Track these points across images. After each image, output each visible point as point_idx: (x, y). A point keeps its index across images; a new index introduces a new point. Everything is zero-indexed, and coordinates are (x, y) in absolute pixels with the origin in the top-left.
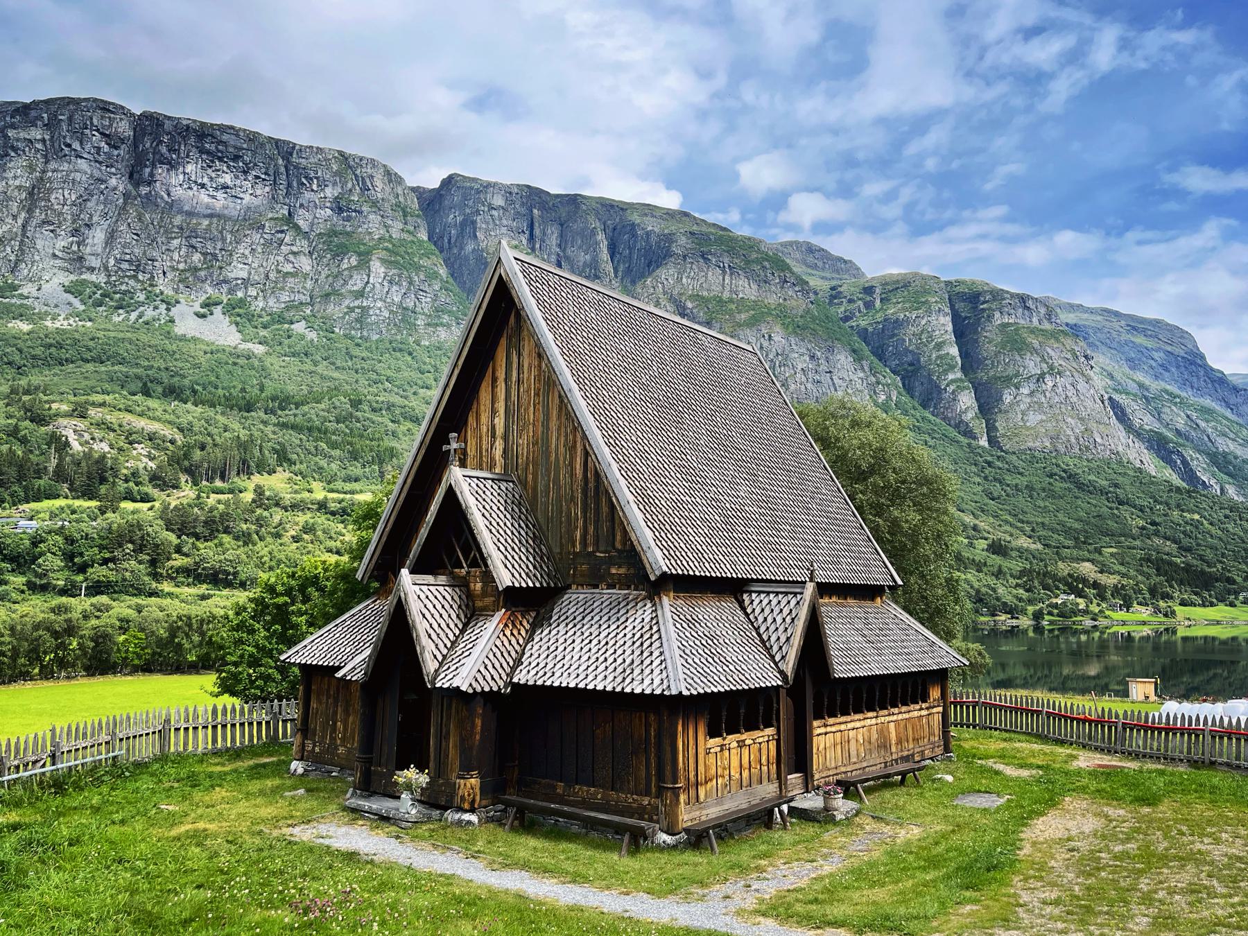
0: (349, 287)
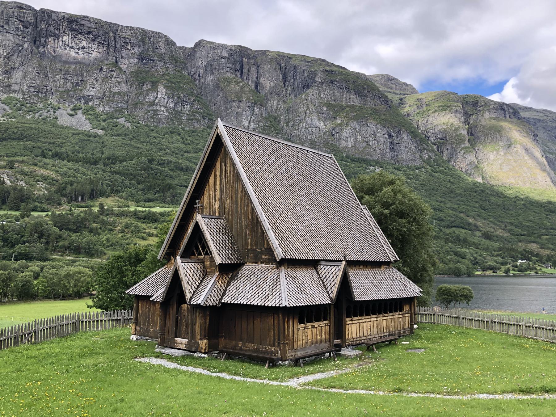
0: (147, 100)
